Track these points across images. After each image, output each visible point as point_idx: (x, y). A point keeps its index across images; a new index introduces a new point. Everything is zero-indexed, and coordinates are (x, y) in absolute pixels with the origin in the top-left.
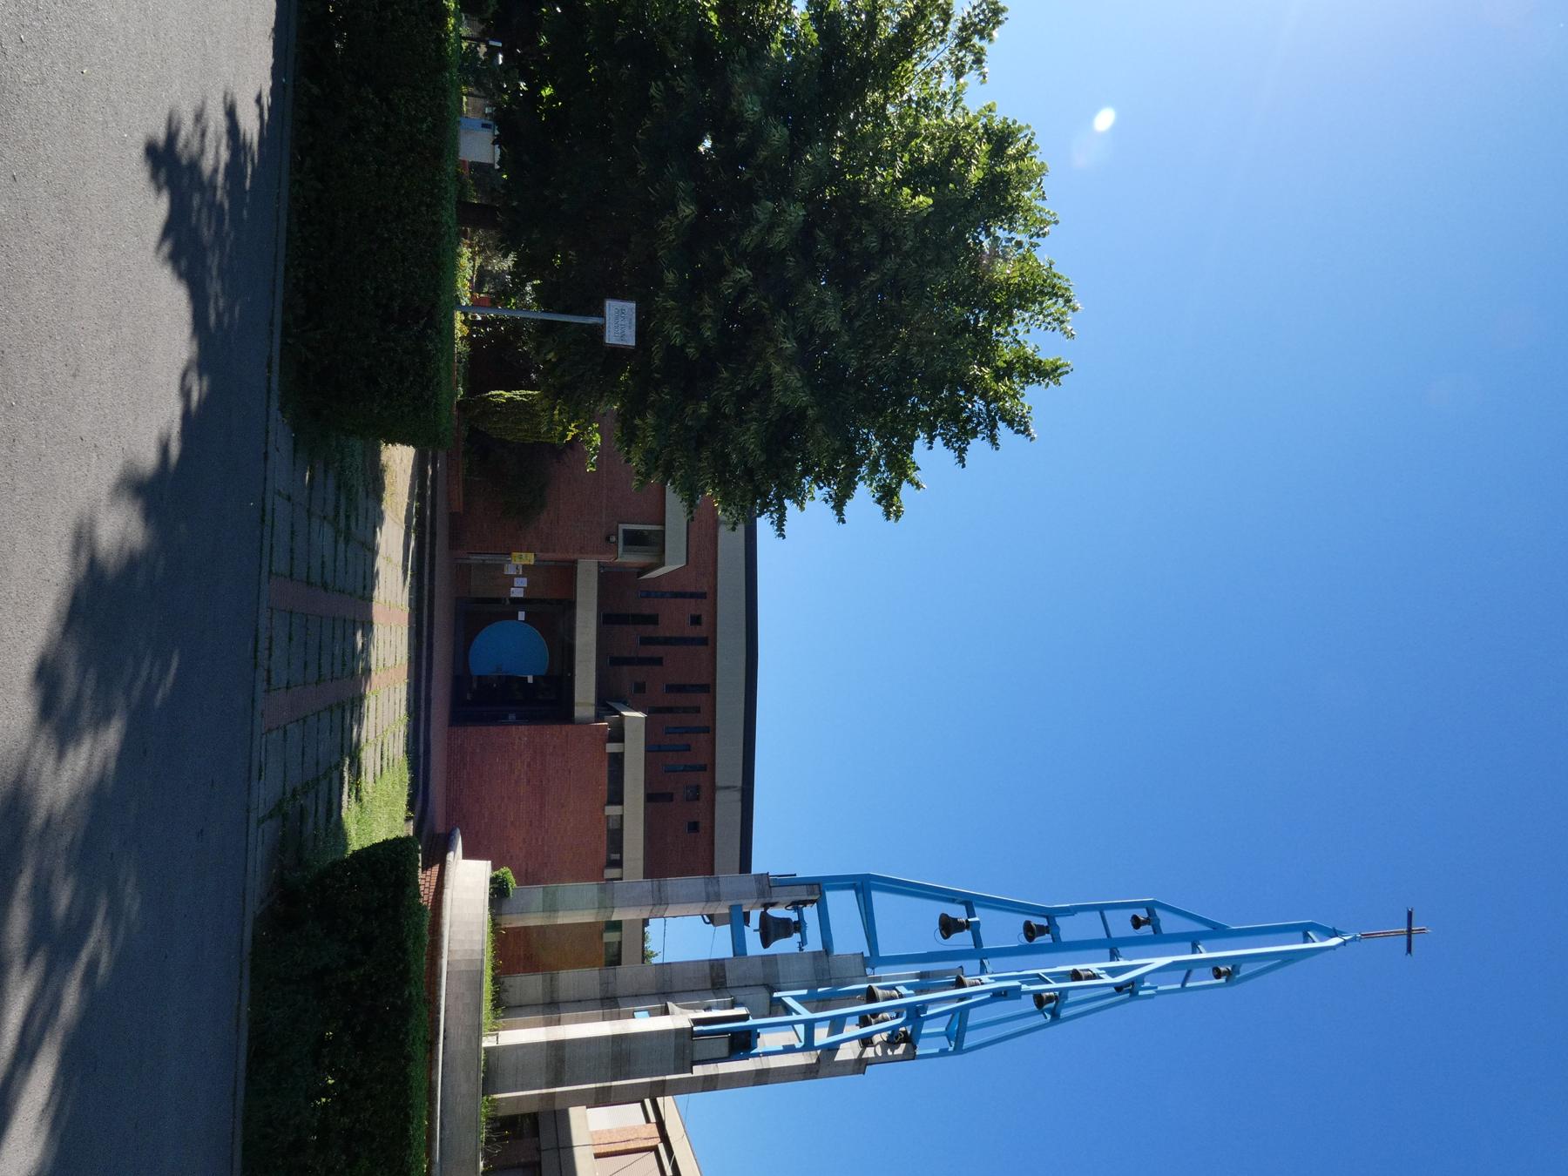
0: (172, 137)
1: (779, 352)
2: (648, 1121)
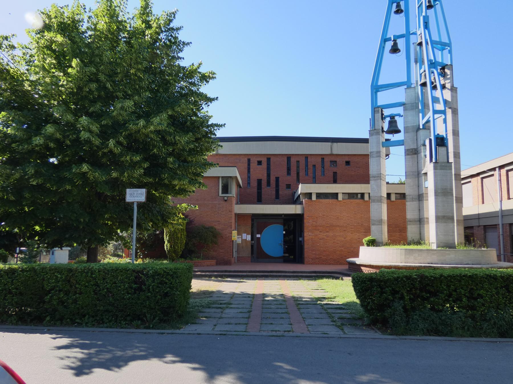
0: (72, 368)
1: (145, 127)
2: (470, 182)
